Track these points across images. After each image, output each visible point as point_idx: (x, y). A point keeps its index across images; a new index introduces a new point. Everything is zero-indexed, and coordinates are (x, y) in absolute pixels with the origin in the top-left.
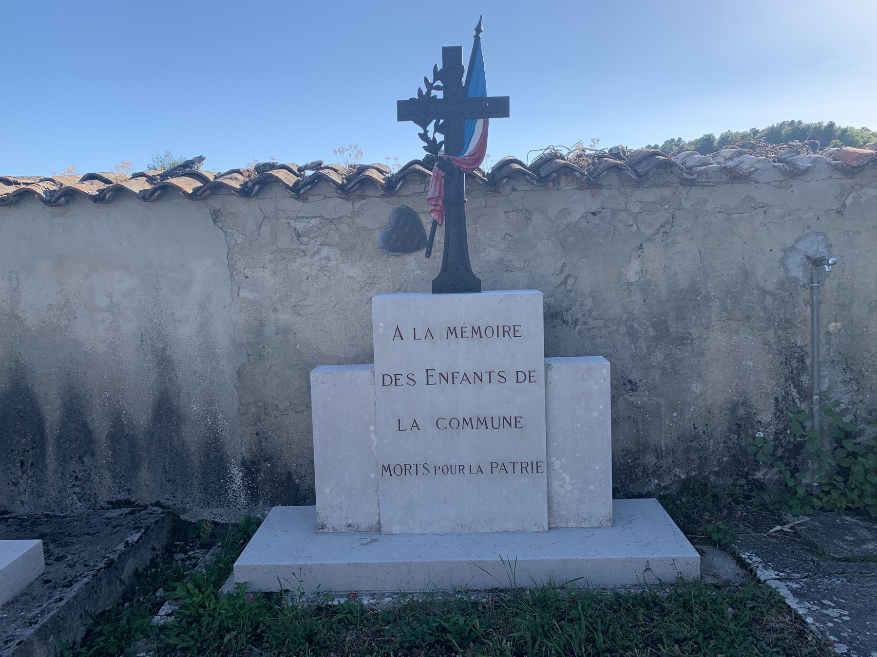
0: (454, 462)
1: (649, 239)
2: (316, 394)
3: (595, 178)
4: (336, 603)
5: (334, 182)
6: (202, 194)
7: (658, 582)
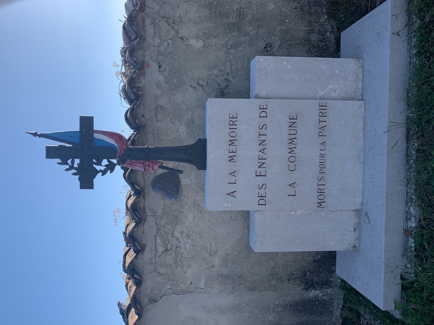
0: (317, 161)
1: (177, 33)
2: (268, 249)
3: (137, 65)
4: (413, 245)
5: (134, 228)
6: (139, 310)
7: (407, 27)
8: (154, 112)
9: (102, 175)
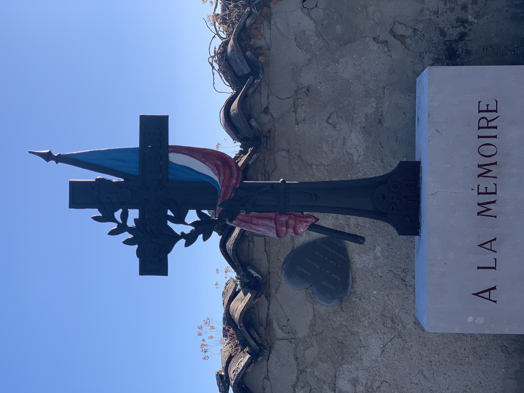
5: (247, 365)
8: (291, 101)
9: (187, 245)
